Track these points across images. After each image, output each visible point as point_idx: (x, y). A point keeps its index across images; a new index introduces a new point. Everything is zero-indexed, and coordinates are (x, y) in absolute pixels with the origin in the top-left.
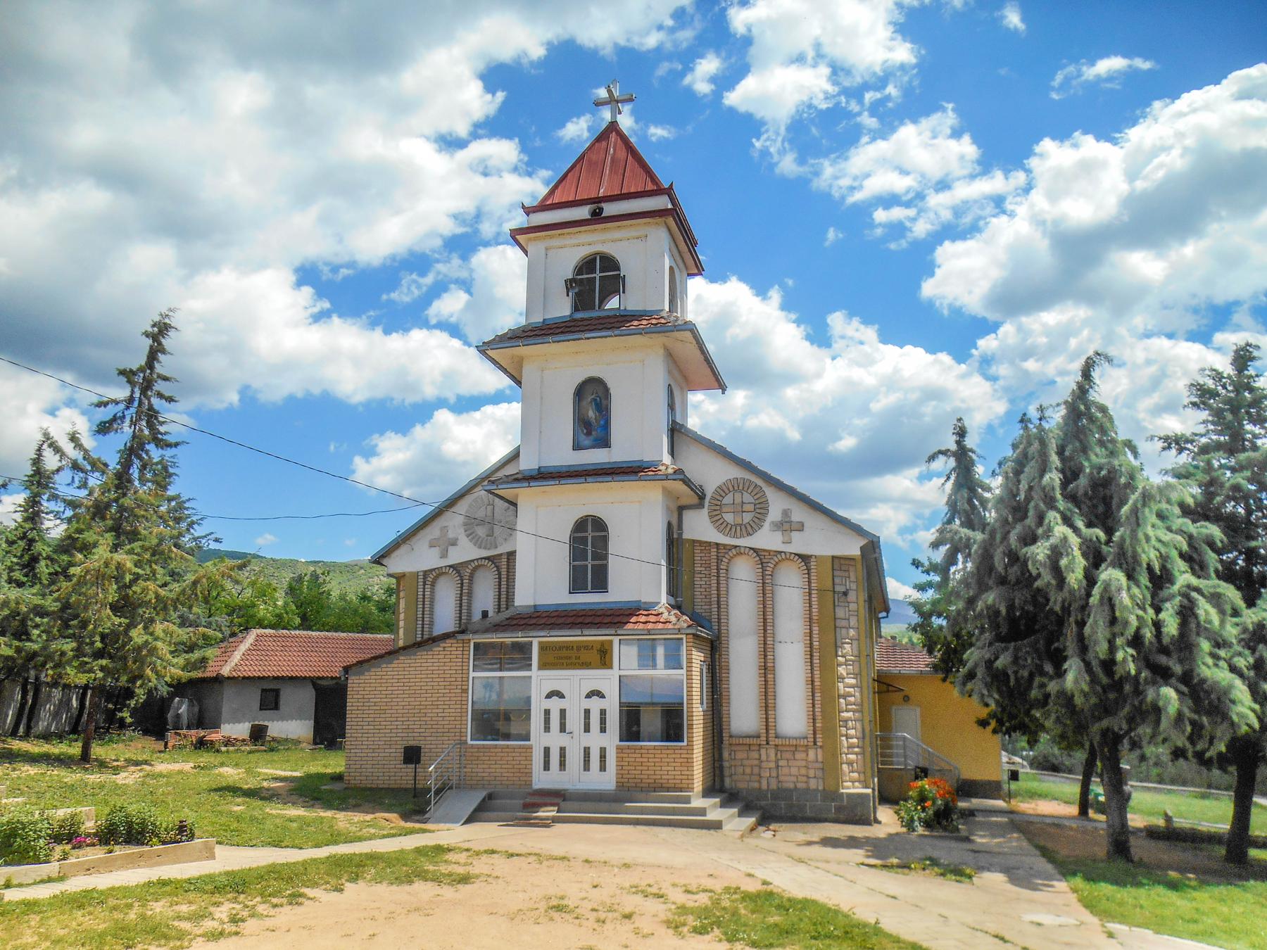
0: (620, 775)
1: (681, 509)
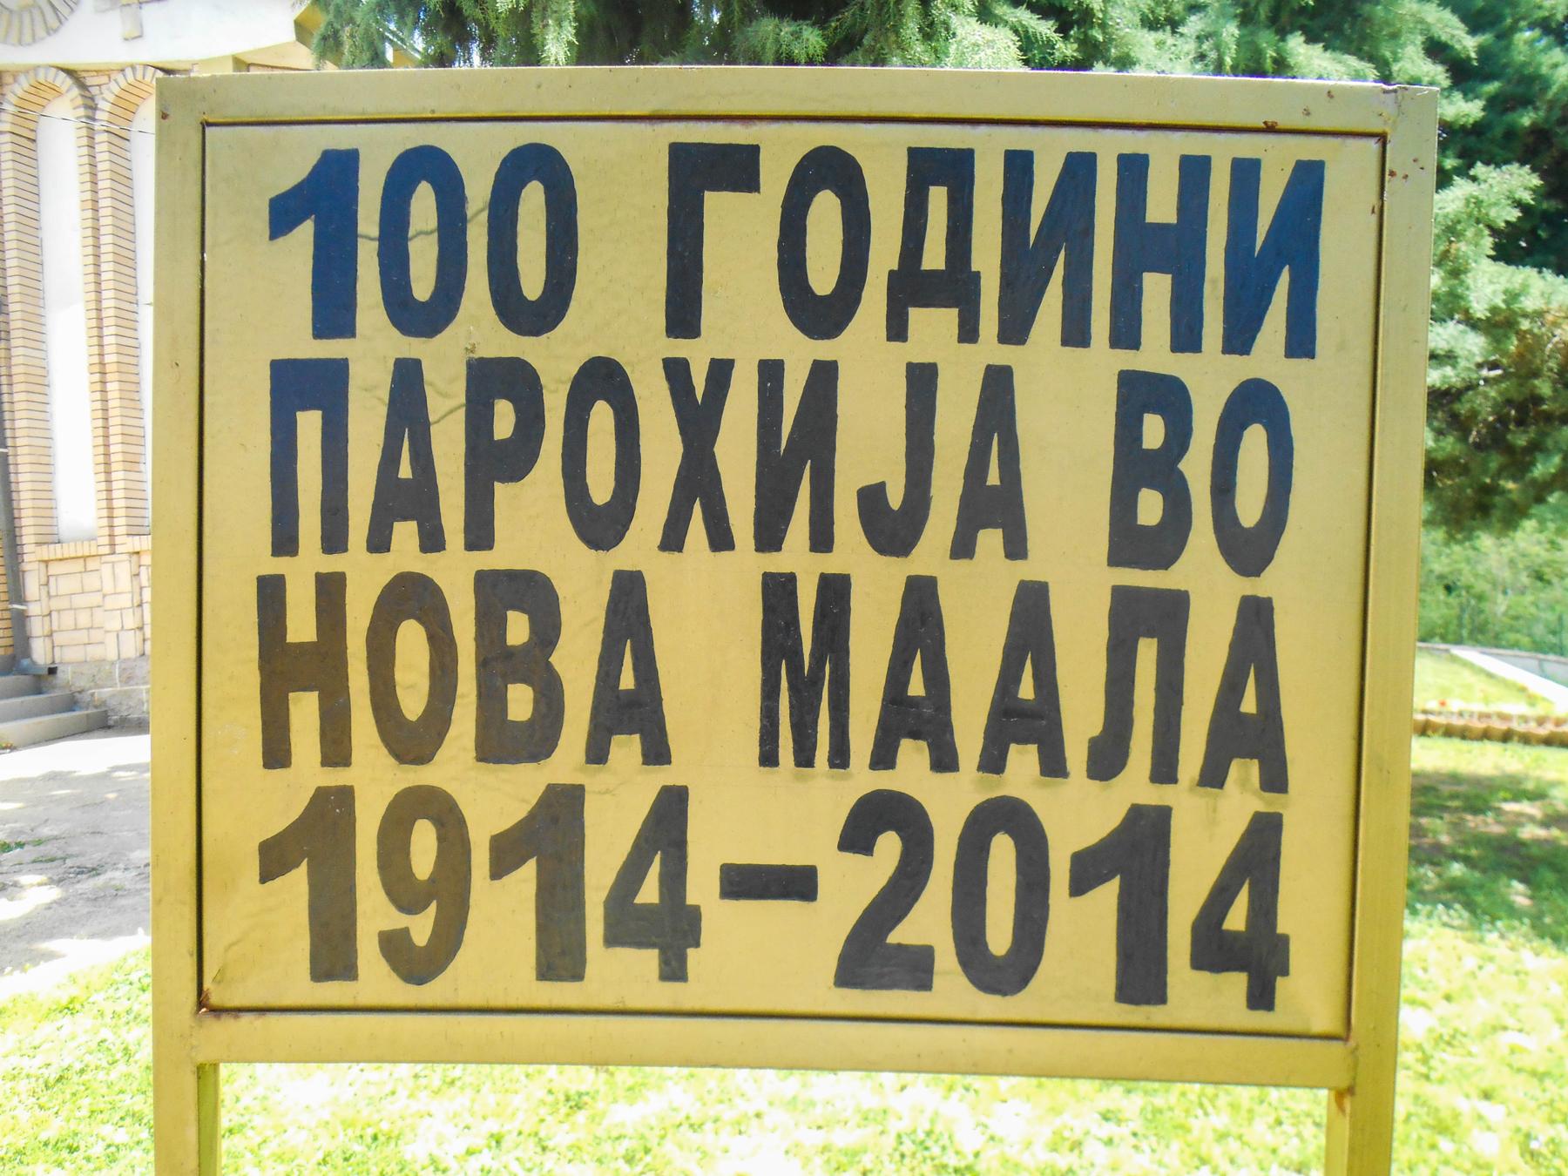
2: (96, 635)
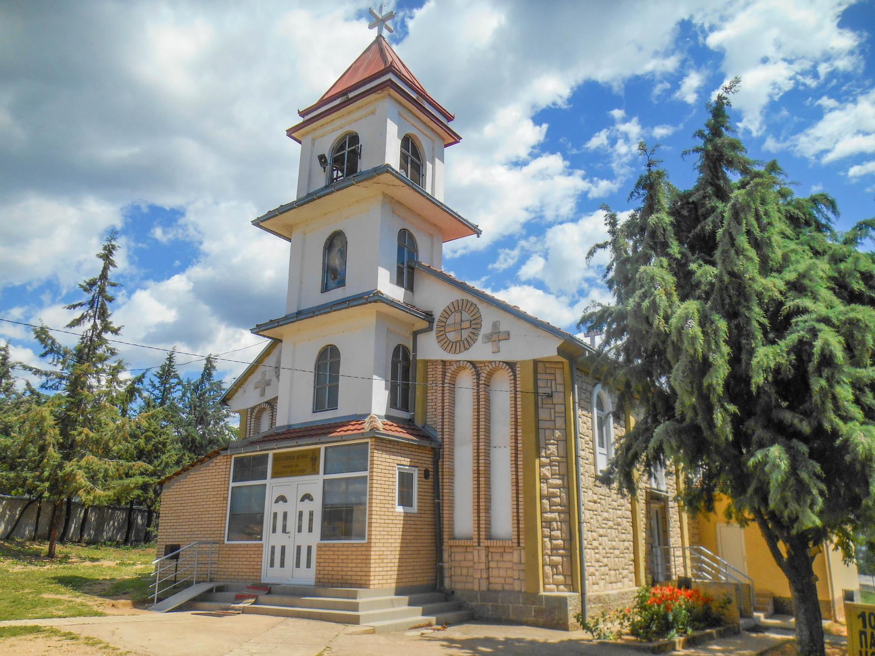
0: (318, 572)
1: (415, 334)
2: (470, 579)
